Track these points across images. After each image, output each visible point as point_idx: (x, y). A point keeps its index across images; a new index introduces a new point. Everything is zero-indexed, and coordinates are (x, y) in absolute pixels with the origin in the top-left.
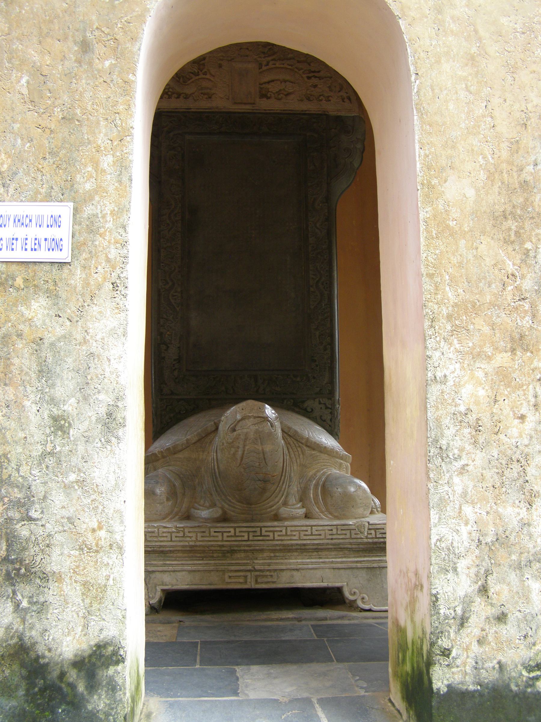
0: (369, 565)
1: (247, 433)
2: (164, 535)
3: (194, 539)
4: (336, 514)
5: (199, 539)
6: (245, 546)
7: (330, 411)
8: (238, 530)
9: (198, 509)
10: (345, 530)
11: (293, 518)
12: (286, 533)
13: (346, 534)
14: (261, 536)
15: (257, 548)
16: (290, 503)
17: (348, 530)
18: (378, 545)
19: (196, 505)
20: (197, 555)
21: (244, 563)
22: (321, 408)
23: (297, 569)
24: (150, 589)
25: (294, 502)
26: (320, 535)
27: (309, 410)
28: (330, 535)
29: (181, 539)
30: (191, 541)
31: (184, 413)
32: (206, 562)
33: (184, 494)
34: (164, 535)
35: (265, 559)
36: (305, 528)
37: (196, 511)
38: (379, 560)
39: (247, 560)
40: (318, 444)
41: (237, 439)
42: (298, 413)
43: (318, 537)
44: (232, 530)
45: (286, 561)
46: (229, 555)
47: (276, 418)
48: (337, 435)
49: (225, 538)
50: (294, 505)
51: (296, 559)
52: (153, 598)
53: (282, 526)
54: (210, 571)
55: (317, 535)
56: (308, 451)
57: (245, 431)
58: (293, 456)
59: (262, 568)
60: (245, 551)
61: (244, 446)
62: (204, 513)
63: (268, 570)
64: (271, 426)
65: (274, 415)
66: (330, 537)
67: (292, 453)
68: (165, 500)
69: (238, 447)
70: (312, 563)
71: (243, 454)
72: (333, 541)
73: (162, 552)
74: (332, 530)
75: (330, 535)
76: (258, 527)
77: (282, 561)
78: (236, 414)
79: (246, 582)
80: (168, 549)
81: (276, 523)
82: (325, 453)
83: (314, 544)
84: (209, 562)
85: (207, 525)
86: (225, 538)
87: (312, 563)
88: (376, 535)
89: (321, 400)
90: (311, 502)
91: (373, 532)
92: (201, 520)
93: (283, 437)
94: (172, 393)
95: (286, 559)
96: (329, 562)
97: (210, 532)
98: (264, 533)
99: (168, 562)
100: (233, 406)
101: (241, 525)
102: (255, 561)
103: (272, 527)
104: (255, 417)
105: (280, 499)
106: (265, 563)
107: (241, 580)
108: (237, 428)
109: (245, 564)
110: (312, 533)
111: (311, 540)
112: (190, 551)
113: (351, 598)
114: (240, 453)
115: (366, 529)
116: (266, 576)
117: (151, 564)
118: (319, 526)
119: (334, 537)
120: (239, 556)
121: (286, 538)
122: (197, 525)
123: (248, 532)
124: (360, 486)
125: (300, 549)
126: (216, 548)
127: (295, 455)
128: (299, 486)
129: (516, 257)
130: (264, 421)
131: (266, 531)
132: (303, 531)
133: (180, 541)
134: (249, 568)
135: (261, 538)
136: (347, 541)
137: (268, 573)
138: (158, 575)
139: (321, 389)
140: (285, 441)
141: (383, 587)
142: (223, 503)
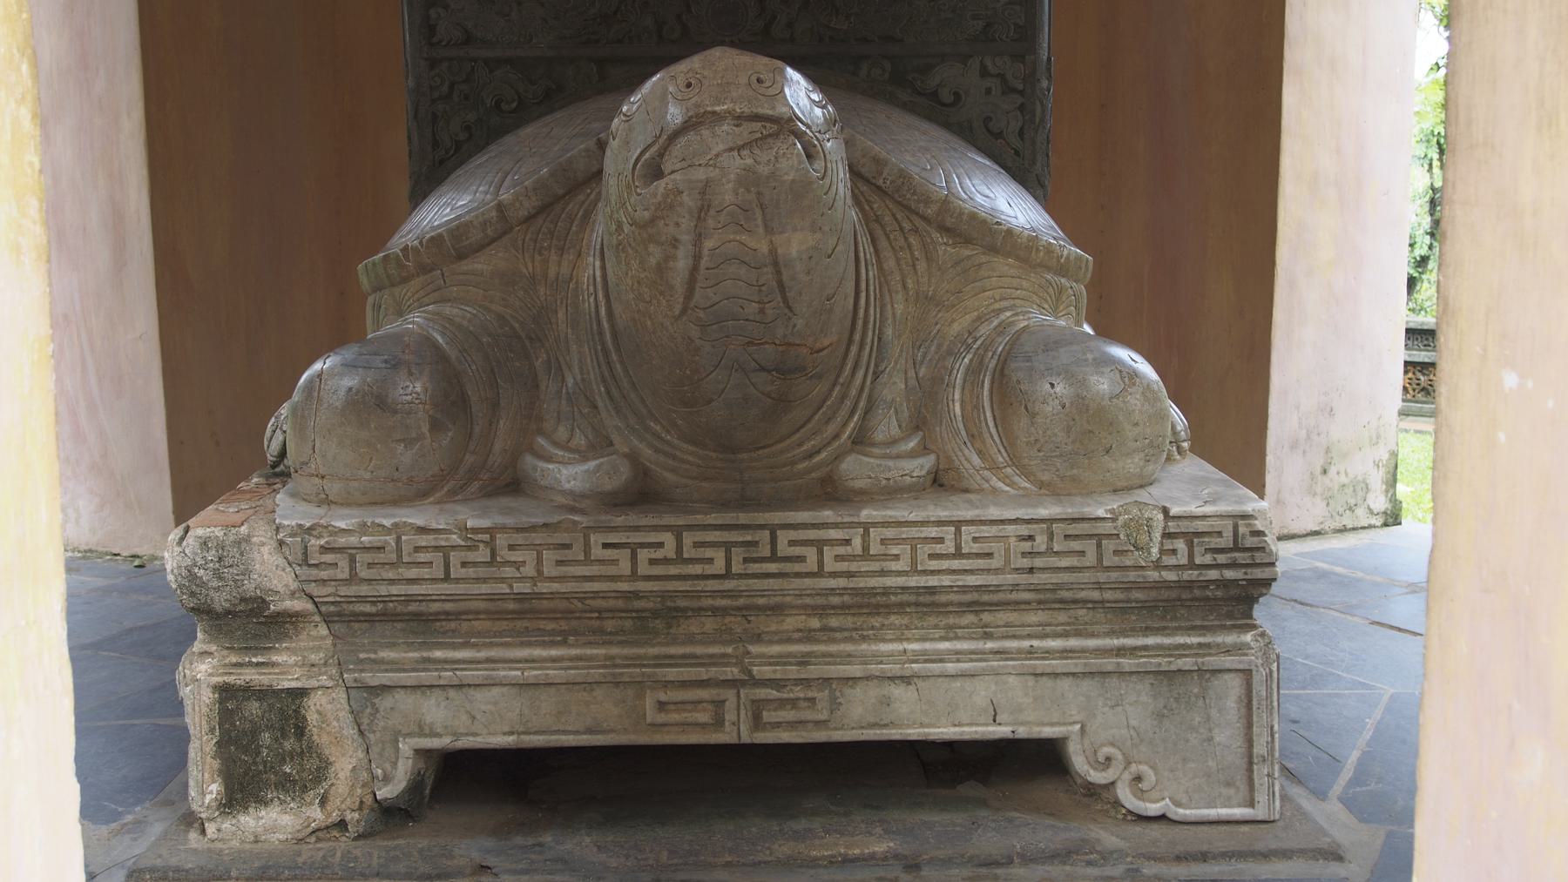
0: (1164, 663)
1: (706, 188)
2: (422, 557)
3: (529, 570)
4: (1046, 477)
5: (548, 570)
6: (715, 594)
7: (1019, 100)
8: (688, 539)
9: (549, 459)
10: (1077, 537)
11: (891, 492)
12: (866, 548)
13: (1082, 553)
14: (774, 558)
15: (761, 601)
16: (879, 436)
17: (1090, 536)
18: (1197, 593)
19: (541, 441)
20: (542, 624)
21: (712, 656)
22: (988, 91)
23: (902, 678)
24: (375, 750)
25: (895, 431)
26: (989, 555)
27: (946, 96)
28: (1024, 554)
29: (482, 572)
30: (521, 579)
31: (514, 111)
32: (574, 652)
33: (495, 405)
34: (422, 557)
35: (789, 641)
36: (933, 532)
37: (542, 464)
38: (1200, 645)
39: (724, 643)
40: (984, 222)
41: (671, 207)
42: (908, 107)
43: (981, 563)
44: (668, 539)
45: (864, 646)
46: (659, 624)
47: (830, 122)
48: (1042, 186)
49: (643, 569)
50: (894, 442)
51: (900, 640)
52: (387, 779)
53: (851, 525)
54: (588, 685)
55: (978, 556)
56: (946, 250)
57: (700, 174)
58: (890, 264)
59: (776, 672)
60: (715, 611)
61: (698, 240)
62: (570, 475)
63: (799, 682)
64: (809, 156)
65: (818, 112)
66: (1026, 563)
67: (887, 253)
68: (425, 429)
69: (675, 243)
70: (958, 655)
71: (694, 269)
72: (1036, 579)
73: (417, 617)
74: (1031, 538)
75: (1024, 554)
76: (762, 527)
77: (849, 647)
78: (664, 103)
79: (719, 723)
80: (435, 607)
81: (828, 515)
82: (1008, 255)
83: (965, 589)
84: (589, 651)
85: (575, 522)
86: (643, 569)
87: (958, 655)
88: (1191, 556)
89: (989, 63)
90: (958, 433)
91: (1180, 545)
92: (560, 499)
93: (854, 196)
94: (469, 39)
95: (864, 638)
96: (1020, 651)
97: (587, 545)
98: (783, 549)
99: (438, 654)
100: (653, 74)
101: (700, 519)
102: (754, 649)
103: (814, 526)
104: (740, 119)
105: (845, 424)
106: (790, 655)
107: (703, 717)
108: (667, 166)
109: (714, 660)
110: (958, 547)
111: (954, 572)
112: (520, 614)
113: (1097, 777)
114: (682, 264)
115: (1157, 535)
116: (793, 703)
117: (375, 661)
118: (983, 522)
119: (1038, 562)
120: (694, 629)
121: (865, 566)
122: (540, 520)
123: (728, 547)
124: (1134, 375)
125: (917, 604)
126: (611, 603)
127: (898, 260)
128: (911, 373)
129: (193, 594)
130: (775, 135)
131: (792, 543)
132: (926, 540)
133: (478, 580)
134: (733, 672)
135: (772, 567)
136: (1086, 577)
137: (798, 692)
138: (405, 701)
139: (988, 25)
140: (862, 209)
141: (1210, 739)
142: (636, 442)
